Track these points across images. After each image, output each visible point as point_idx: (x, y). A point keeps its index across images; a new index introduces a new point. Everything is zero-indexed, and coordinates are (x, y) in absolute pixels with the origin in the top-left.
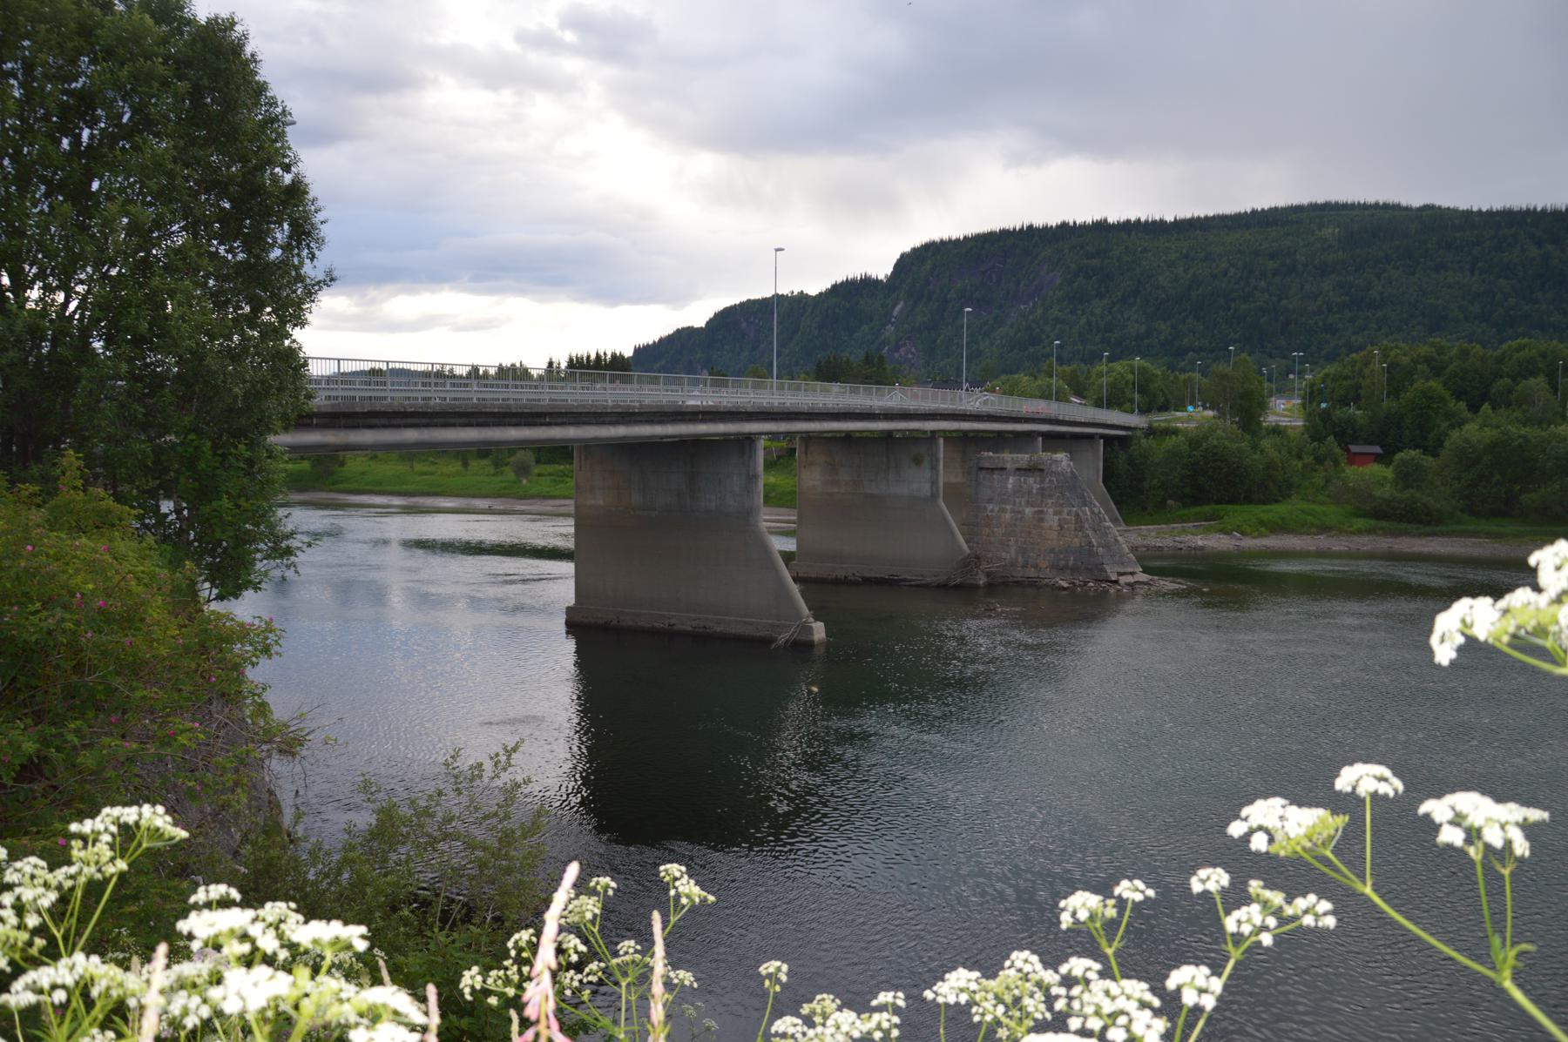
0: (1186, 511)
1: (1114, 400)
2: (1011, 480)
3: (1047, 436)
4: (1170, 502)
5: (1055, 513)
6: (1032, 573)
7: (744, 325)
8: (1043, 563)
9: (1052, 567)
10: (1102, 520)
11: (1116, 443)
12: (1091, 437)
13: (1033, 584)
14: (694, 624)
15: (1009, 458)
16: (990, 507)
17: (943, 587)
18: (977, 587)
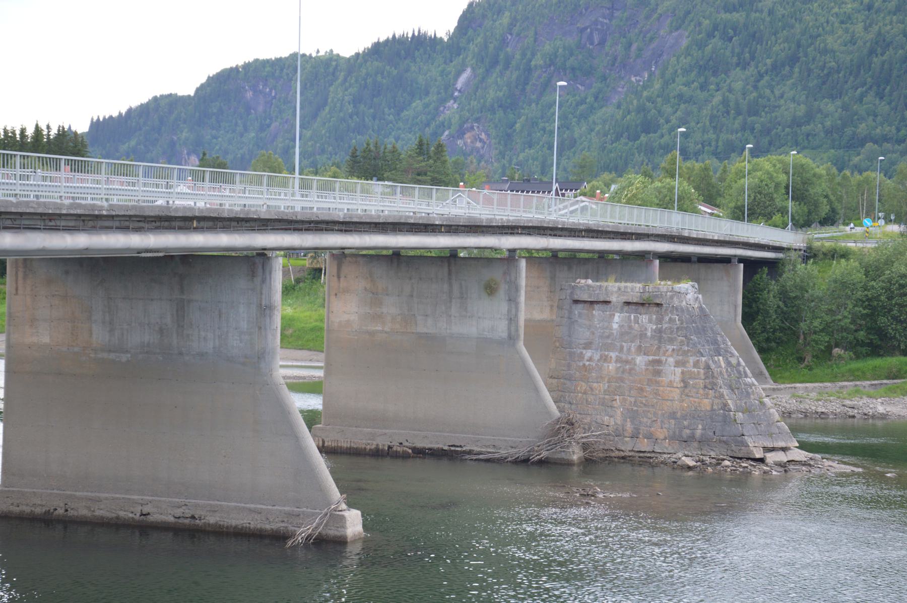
0: (855, 365)
1: (757, 210)
2: (617, 317)
3: (667, 259)
4: (837, 351)
5: (678, 364)
6: (644, 445)
7: (249, 94)
8: (660, 434)
9: (672, 438)
10: (741, 375)
11: (759, 269)
12: (725, 260)
13: (645, 460)
14: (178, 512)
15: (614, 288)
16: (588, 354)
17: (524, 462)
18: (569, 464)
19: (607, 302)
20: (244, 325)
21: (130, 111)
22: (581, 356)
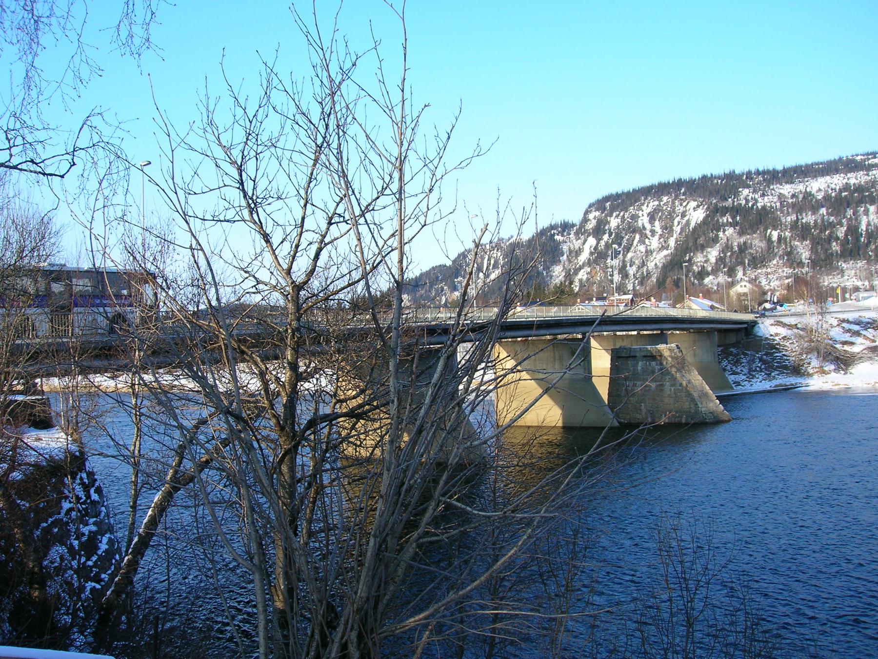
19: (635, 357)
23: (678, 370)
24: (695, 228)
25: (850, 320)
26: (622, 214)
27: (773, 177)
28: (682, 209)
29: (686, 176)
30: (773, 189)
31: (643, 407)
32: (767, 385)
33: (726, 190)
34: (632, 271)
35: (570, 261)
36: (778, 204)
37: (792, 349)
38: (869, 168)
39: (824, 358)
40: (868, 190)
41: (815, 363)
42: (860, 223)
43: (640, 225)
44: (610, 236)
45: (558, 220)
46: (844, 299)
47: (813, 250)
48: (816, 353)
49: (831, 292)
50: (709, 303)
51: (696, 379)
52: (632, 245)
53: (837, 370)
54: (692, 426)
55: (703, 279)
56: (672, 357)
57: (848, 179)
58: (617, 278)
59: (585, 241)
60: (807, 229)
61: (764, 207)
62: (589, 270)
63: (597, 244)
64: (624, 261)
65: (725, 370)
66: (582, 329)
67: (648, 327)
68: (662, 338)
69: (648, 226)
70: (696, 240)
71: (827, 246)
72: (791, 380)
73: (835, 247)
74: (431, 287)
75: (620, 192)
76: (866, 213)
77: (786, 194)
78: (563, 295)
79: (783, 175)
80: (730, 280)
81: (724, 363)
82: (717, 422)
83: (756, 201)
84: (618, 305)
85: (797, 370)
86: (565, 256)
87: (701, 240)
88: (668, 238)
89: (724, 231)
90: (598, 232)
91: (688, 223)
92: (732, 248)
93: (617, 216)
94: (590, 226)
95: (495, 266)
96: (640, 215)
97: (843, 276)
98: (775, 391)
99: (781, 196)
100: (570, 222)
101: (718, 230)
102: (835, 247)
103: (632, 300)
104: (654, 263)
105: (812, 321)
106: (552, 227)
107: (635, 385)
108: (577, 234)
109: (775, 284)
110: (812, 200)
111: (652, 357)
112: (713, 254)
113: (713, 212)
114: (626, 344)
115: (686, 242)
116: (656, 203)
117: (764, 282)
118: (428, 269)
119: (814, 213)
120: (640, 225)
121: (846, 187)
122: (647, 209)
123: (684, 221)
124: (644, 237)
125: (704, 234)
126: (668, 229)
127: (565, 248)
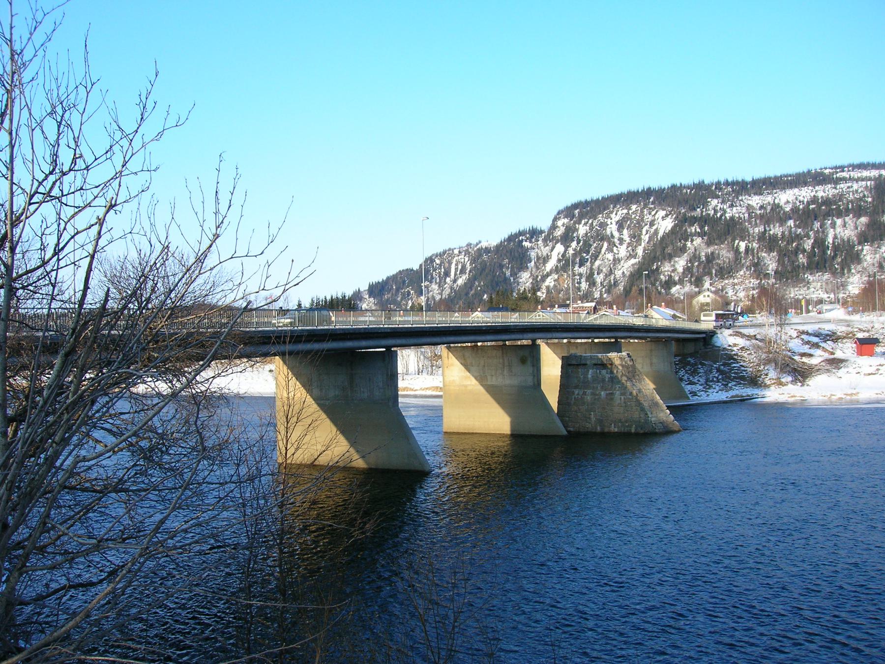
19: (585, 365)
20: (381, 384)
21: (388, 278)
22: (573, 393)
23: (629, 379)
24: (663, 238)
25: (810, 332)
26: (590, 221)
27: (742, 188)
28: (650, 218)
29: (655, 185)
30: (742, 200)
31: (592, 416)
32: (723, 396)
33: (694, 200)
34: (599, 279)
35: (537, 268)
36: (746, 215)
37: (750, 360)
38: (837, 181)
39: (781, 370)
40: (835, 203)
41: (772, 374)
42: (827, 236)
43: (608, 232)
44: (578, 243)
45: (526, 225)
46: (808, 311)
47: (780, 261)
48: (773, 364)
49: (797, 305)
50: (672, 312)
51: (648, 386)
52: (600, 253)
53: (794, 382)
54: (641, 436)
55: (670, 288)
56: (623, 366)
57: (816, 192)
58: (584, 285)
59: (553, 248)
60: (774, 241)
61: (732, 218)
62: (556, 277)
63: (565, 252)
64: (591, 269)
65: (681, 380)
66: (531, 335)
67: (601, 334)
68: (616, 347)
69: (616, 234)
70: (664, 248)
71: (793, 258)
72: (748, 391)
73: (802, 259)
74: (398, 290)
75: (589, 199)
76: (833, 225)
77: (755, 205)
78: (528, 300)
79: (752, 187)
80: (697, 289)
81: (682, 373)
82: (668, 432)
83: (725, 212)
84: (581, 314)
85: (754, 381)
86: (533, 263)
87: (669, 250)
88: (636, 247)
89: (692, 241)
90: (566, 239)
91: (656, 232)
92: (700, 258)
93: (586, 224)
94: (559, 232)
95: (463, 271)
96: (609, 223)
97: (808, 288)
98: (731, 402)
99: (749, 207)
100: (539, 228)
101: (686, 240)
102: (802, 259)
103: (595, 308)
104: (621, 271)
105: (771, 332)
106: (521, 233)
107: (585, 393)
108: (545, 241)
109: (742, 295)
110: (780, 212)
111: (602, 365)
112: (681, 263)
113: (682, 221)
114: (579, 352)
115: (654, 251)
116: (625, 211)
117: (730, 293)
118: (395, 273)
119: (781, 225)
120: (608, 232)
121: (814, 200)
122: (616, 217)
123: (652, 230)
124: (612, 245)
125: (672, 244)
126: (636, 237)
127: (533, 254)
